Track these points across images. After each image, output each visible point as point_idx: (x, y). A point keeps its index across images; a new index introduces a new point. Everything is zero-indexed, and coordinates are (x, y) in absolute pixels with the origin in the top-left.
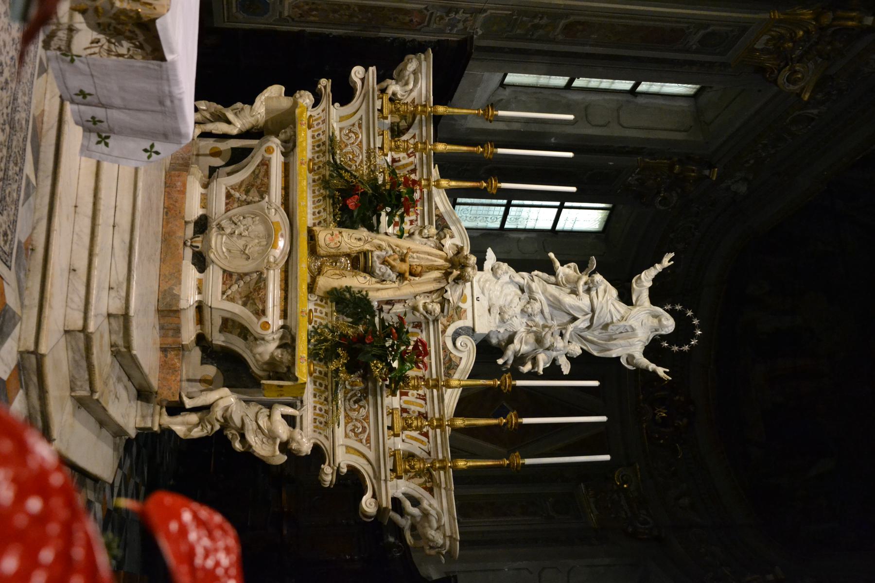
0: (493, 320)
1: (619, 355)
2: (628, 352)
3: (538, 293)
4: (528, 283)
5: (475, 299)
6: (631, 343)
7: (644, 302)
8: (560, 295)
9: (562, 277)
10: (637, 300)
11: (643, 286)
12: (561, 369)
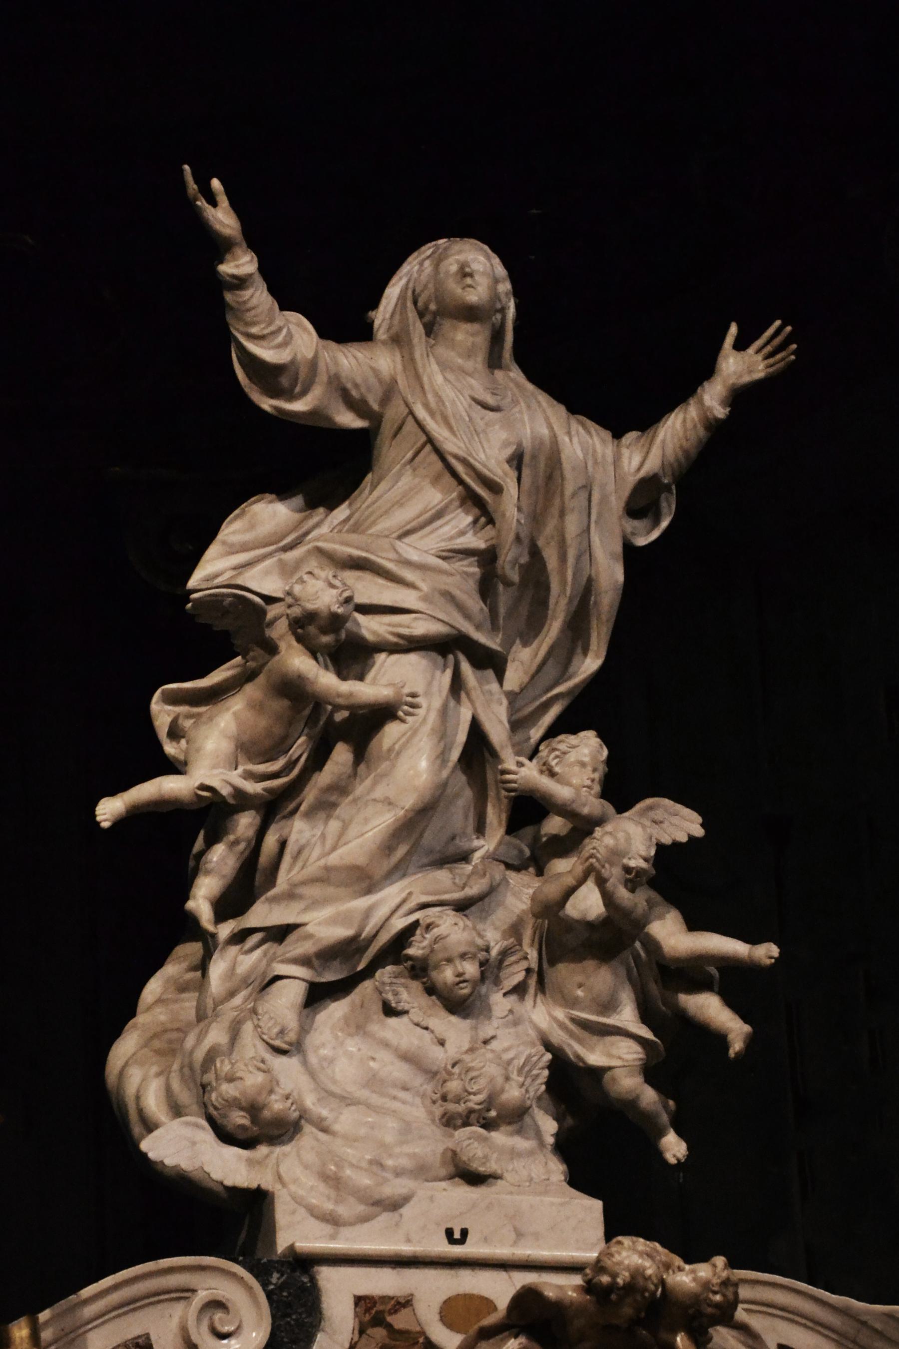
0: (518, 1164)
1: (618, 548)
2: (617, 503)
3: (368, 913)
4: (305, 961)
5: (457, 1251)
6: (581, 482)
7: (376, 372)
8: (389, 803)
9: (250, 776)
10: (357, 406)
11: (313, 364)
12: (676, 844)
